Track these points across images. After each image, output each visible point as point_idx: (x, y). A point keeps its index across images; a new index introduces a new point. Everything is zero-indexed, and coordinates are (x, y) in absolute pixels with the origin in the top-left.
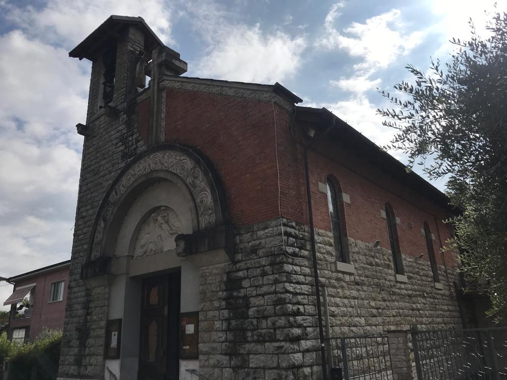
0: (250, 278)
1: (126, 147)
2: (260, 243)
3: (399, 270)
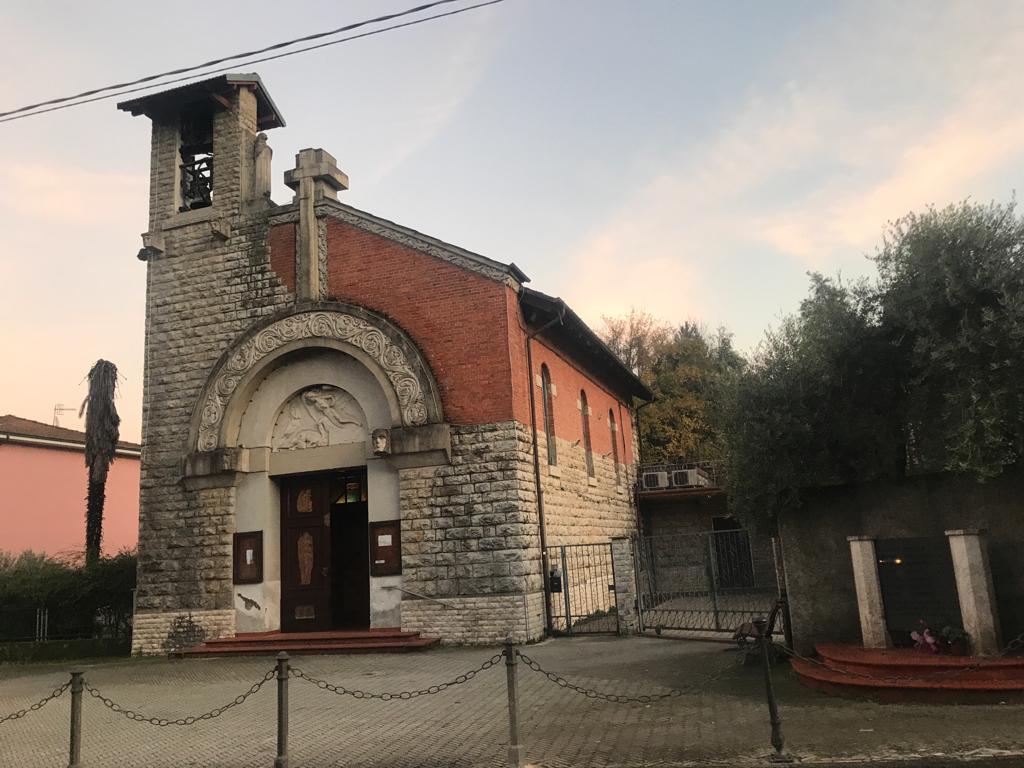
0: (474, 484)
1: (249, 289)
2: (487, 447)
3: (591, 473)
